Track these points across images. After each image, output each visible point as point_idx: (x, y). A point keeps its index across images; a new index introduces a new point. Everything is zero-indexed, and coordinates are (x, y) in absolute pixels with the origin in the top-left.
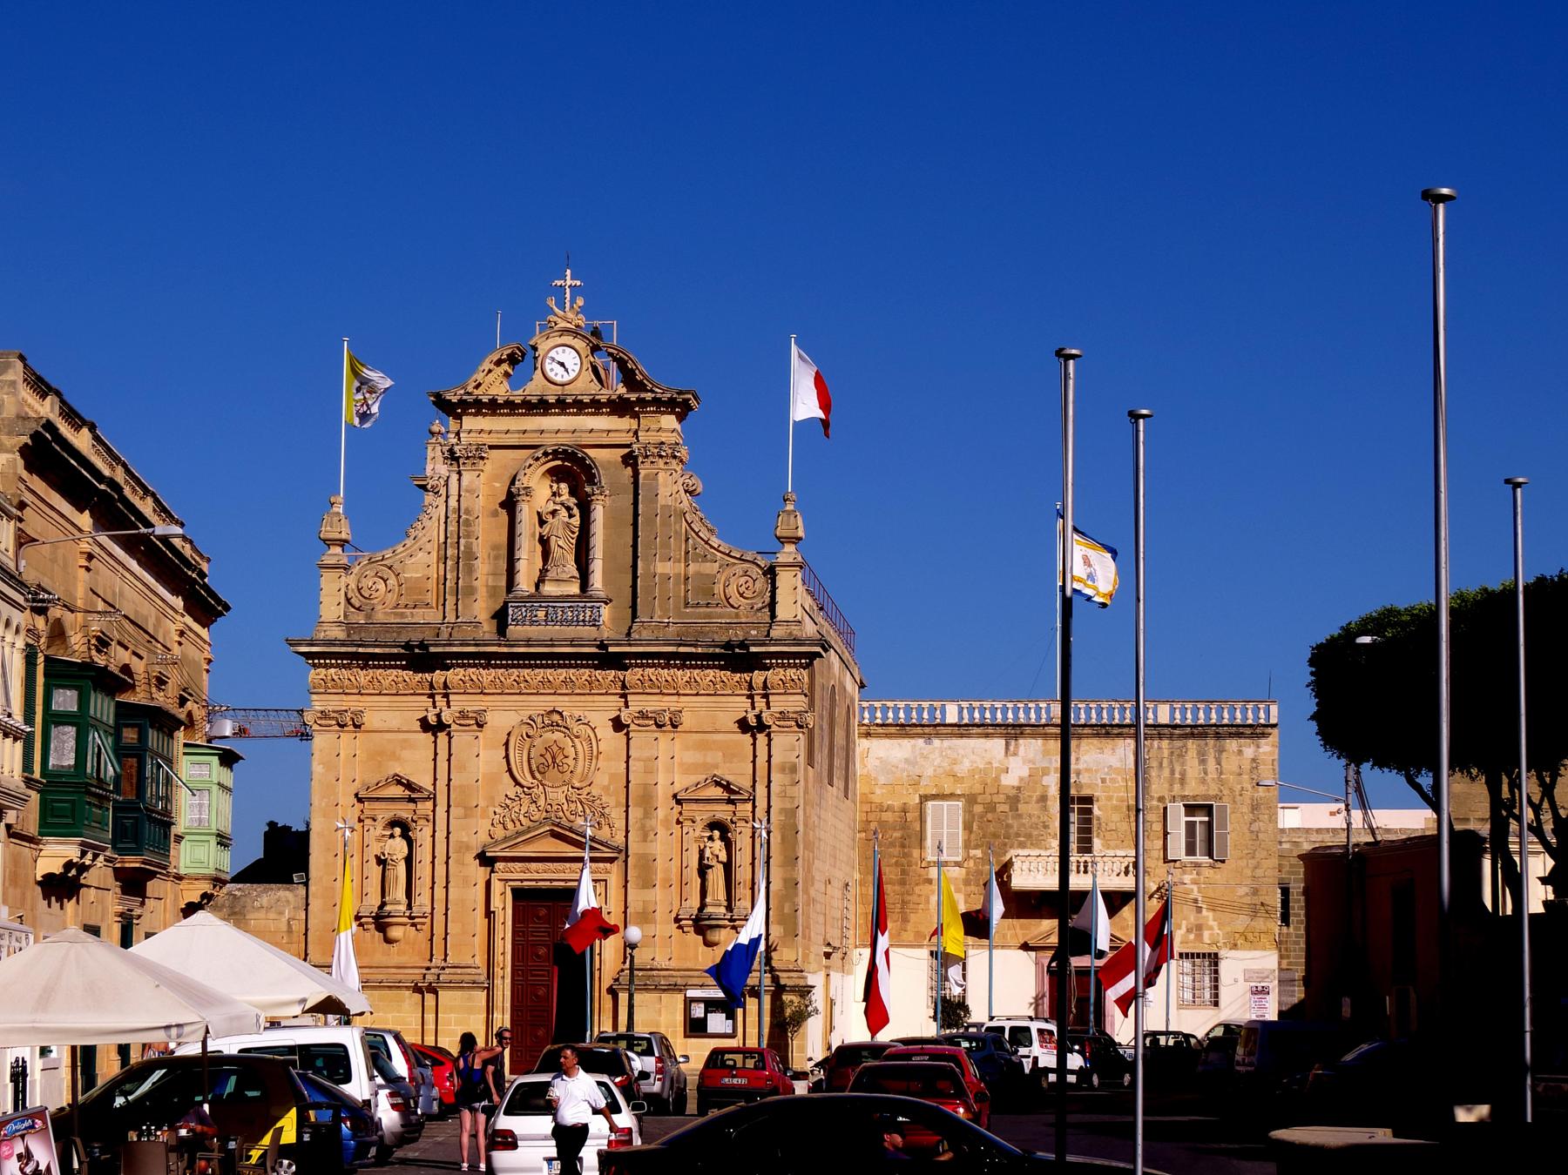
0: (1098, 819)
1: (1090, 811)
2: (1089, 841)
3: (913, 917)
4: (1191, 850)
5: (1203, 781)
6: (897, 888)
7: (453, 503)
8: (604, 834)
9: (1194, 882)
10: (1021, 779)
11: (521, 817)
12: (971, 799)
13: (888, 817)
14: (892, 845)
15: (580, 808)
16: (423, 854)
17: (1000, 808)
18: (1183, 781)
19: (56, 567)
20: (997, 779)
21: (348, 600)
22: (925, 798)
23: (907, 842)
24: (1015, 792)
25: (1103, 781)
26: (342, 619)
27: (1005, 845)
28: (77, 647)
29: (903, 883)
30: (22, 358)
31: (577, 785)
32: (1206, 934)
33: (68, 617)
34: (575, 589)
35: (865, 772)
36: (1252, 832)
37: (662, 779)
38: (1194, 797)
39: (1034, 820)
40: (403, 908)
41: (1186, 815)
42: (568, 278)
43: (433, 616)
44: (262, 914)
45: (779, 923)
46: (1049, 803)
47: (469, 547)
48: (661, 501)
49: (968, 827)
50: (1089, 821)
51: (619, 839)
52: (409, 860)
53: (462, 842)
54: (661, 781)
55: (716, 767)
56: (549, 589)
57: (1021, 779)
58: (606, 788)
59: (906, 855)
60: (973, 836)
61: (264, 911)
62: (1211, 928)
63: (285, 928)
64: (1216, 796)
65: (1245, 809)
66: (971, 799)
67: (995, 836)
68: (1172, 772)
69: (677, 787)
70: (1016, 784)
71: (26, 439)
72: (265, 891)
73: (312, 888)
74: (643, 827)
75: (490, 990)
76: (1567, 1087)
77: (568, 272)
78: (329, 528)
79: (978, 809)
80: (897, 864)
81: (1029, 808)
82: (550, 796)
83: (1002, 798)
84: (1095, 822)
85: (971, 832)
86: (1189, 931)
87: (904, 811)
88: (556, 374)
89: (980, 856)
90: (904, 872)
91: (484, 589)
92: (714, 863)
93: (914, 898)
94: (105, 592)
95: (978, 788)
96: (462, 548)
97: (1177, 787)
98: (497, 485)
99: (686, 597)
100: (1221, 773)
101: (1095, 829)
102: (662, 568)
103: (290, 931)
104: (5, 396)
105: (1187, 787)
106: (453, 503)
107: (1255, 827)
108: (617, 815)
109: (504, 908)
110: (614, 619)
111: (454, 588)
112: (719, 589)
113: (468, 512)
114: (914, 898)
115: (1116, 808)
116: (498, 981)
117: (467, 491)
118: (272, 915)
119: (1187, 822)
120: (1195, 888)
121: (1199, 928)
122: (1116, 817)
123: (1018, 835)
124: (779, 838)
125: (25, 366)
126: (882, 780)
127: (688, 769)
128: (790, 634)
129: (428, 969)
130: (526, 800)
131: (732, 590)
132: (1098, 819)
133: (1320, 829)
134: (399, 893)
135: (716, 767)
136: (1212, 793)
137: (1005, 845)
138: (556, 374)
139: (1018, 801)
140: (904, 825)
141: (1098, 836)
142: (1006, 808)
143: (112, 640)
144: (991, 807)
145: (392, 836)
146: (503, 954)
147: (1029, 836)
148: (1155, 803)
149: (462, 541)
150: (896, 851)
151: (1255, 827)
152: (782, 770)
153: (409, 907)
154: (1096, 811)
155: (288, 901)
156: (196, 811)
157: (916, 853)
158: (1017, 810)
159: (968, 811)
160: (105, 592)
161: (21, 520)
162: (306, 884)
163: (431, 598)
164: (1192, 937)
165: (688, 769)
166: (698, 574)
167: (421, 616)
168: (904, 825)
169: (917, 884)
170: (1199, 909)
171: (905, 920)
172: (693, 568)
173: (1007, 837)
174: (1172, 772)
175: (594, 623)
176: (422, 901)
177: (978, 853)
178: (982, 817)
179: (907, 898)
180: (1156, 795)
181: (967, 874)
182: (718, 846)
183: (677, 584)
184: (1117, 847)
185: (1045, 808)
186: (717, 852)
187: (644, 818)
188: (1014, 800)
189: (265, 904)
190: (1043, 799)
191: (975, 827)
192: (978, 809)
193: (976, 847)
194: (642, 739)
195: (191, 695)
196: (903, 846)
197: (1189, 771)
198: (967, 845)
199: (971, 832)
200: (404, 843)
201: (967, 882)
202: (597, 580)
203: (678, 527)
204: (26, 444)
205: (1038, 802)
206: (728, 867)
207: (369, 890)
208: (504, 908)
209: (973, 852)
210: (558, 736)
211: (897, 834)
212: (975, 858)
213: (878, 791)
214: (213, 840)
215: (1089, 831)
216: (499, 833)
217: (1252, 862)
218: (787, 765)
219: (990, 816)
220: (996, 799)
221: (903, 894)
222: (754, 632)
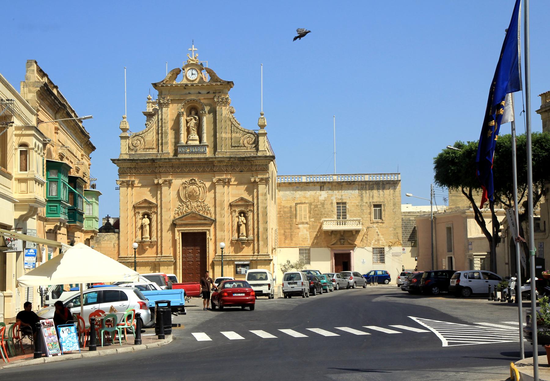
0: (348, 209)
1: (345, 207)
2: (346, 215)
3: (294, 239)
4: (375, 218)
5: (379, 197)
6: (289, 230)
7: (160, 117)
8: (209, 216)
9: (377, 227)
10: (325, 198)
11: (184, 211)
12: (310, 204)
13: (286, 210)
14: (287, 218)
15: (201, 209)
16: (154, 224)
17: (319, 206)
18: (373, 197)
19: (48, 132)
20: (318, 198)
21: (129, 147)
22: (297, 204)
23: (292, 217)
24: (323, 201)
25: (349, 198)
26: (127, 153)
27: (321, 217)
28: (55, 158)
29: (291, 229)
30: (36, 62)
31: (200, 201)
32: (381, 242)
33: (52, 148)
34: (197, 143)
35: (279, 197)
36: (393, 212)
37: (226, 199)
38: (376, 202)
39: (329, 210)
40: (148, 239)
41: (374, 207)
42: (193, 48)
43: (155, 151)
44: (105, 242)
45: (262, 241)
46: (333, 204)
47: (165, 130)
48: (223, 115)
49: (310, 212)
50: (346, 210)
51: (213, 218)
52: (150, 225)
53: (166, 219)
54: (225, 199)
55: (242, 194)
56: (190, 143)
57: (325, 198)
58: (209, 202)
59: (291, 221)
60: (311, 215)
61: (106, 241)
62: (382, 240)
63: (113, 246)
64: (383, 202)
65: (392, 205)
66: (310, 204)
67: (318, 214)
68: (370, 195)
69: (230, 201)
70: (323, 199)
71: (39, 89)
72: (106, 235)
73: (121, 234)
74: (220, 213)
75: (175, 264)
76: (549, 289)
77: (193, 46)
78: (122, 125)
79: (313, 207)
80: (289, 223)
81: (327, 206)
82: (192, 204)
83: (319, 203)
84: (347, 210)
85: (311, 213)
86: (376, 241)
87: (291, 208)
88: (189, 76)
89: (313, 220)
90: (291, 226)
91: (171, 143)
92: (241, 223)
93: (294, 233)
94: (62, 141)
95: (312, 201)
96: (163, 131)
97: (371, 199)
98: (174, 111)
99: (232, 144)
100: (384, 195)
101: (347, 212)
102: (224, 135)
103: (114, 247)
104: (31, 75)
105: (374, 199)
106: (160, 117)
107: (394, 210)
108: (212, 209)
109: (179, 239)
110: (210, 151)
111: (160, 143)
112: (241, 142)
113: (165, 119)
114: (294, 233)
115: (353, 206)
116: (178, 260)
117: (165, 113)
118: (108, 242)
119: (374, 209)
120: (377, 229)
121: (378, 240)
122: (353, 208)
123: (324, 214)
124: (262, 216)
125: (37, 65)
126: (284, 199)
127: (233, 196)
128: (263, 154)
129: (157, 257)
130: (185, 206)
131: (245, 142)
132: (348, 209)
133: (409, 212)
134: (147, 235)
135: (242, 194)
136: (381, 201)
137: (321, 217)
138: (189, 76)
139: (324, 204)
140: (291, 212)
141: (348, 214)
142: (321, 206)
143: (65, 156)
144: (316, 206)
145: (145, 218)
146: (179, 252)
147: (328, 214)
148: (365, 204)
149: (164, 129)
150: (288, 220)
151: (394, 210)
152: (262, 195)
153: (150, 239)
154: (347, 207)
155: (113, 238)
156: (88, 211)
157: (294, 220)
158: (324, 207)
159: (310, 208)
160: (62, 141)
161: (38, 115)
162: (119, 233)
163: (155, 146)
164: (376, 243)
165: (233, 196)
166: (235, 137)
167: (151, 152)
168: (291, 212)
169: (295, 229)
170: (378, 235)
171: (292, 240)
172: (234, 135)
173: (321, 215)
174: (370, 195)
175: (204, 153)
176: (154, 238)
177: (313, 220)
178: (314, 209)
179: (292, 233)
180: (365, 202)
181: (310, 226)
182: (243, 218)
183: (229, 140)
184: (354, 217)
185: (332, 206)
186: (243, 220)
187: (221, 210)
188: (323, 204)
189: (106, 239)
190: (332, 203)
191: (312, 212)
192: (313, 207)
193: (312, 218)
194: (219, 188)
195: (86, 175)
196: (291, 218)
197: (375, 194)
198: (310, 217)
199: (311, 213)
200: (148, 220)
201: (310, 228)
202: (205, 140)
203: (229, 123)
204: (39, 90)
205: (330, 204)
206: (246, 224)
207: (138, 234)
208: (179, 239)
209: (311, 220)
210: (194, 186)
211: (289, 215)
212: (312, 221)
213: (283, 202)
214: (442, 198)
215: (345, 212)
216: (177, 217)
217: (394, 221)
218: (263, 194)
219: (316, 209)
220: (318, 204)
221: (291, 232)
222: (252, 154)
